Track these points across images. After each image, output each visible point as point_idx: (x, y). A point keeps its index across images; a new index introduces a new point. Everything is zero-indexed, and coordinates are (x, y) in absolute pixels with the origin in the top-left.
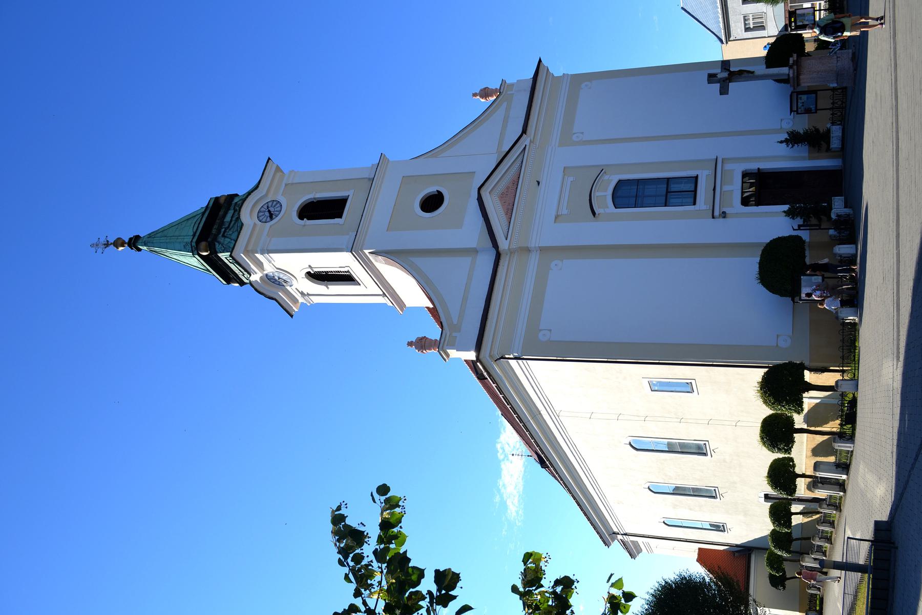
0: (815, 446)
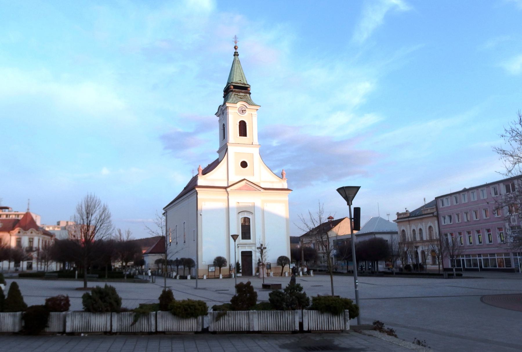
0: (150, 236)
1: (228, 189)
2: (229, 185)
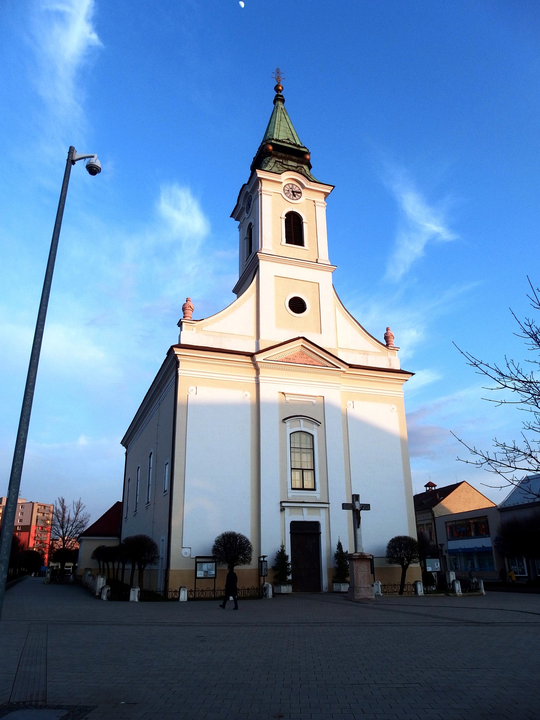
1: (259, 358)
2: (261, 349)
